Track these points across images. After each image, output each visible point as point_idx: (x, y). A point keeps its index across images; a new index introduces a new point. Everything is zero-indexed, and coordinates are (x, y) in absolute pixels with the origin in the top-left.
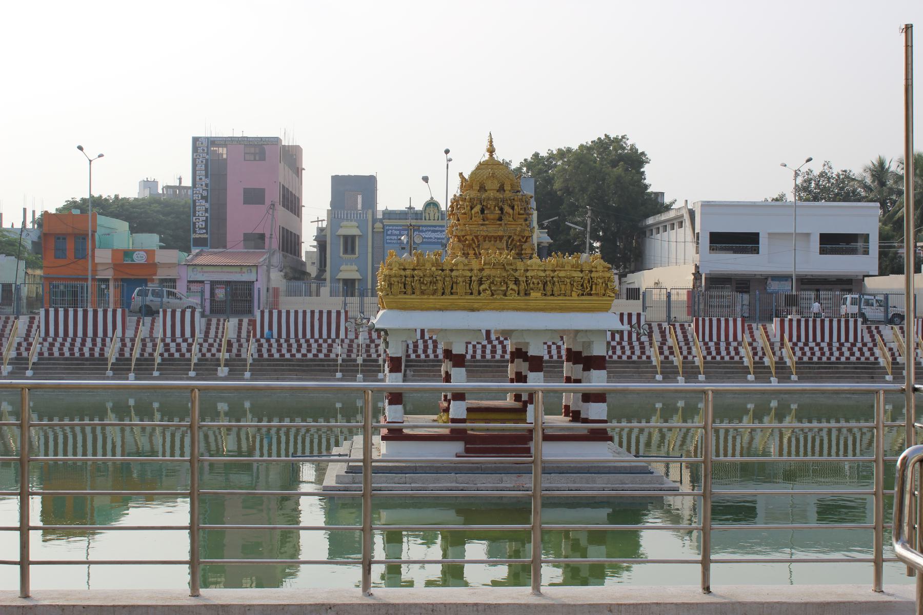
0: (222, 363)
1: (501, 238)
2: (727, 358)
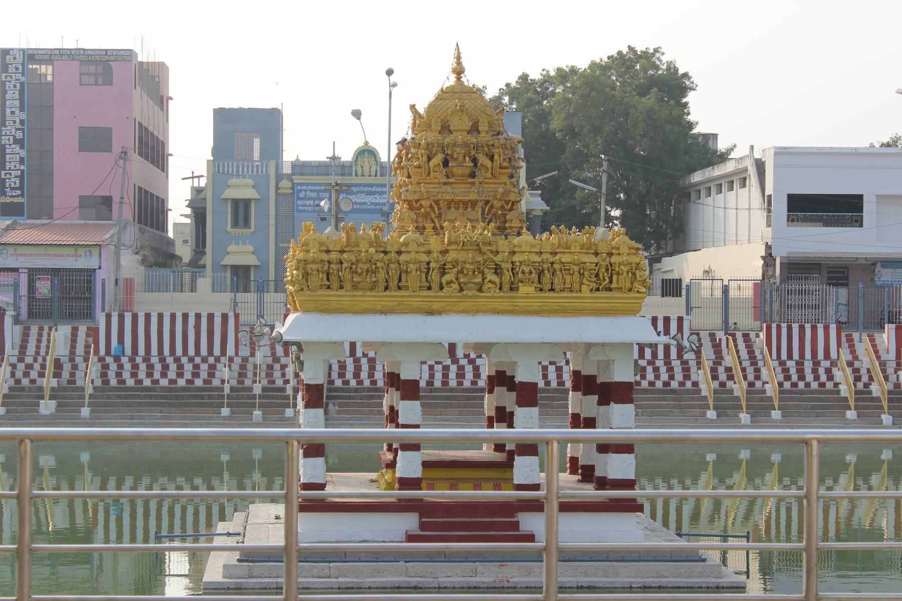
0: (47, 393)
1: (474, 203)
2: (815, 385)
